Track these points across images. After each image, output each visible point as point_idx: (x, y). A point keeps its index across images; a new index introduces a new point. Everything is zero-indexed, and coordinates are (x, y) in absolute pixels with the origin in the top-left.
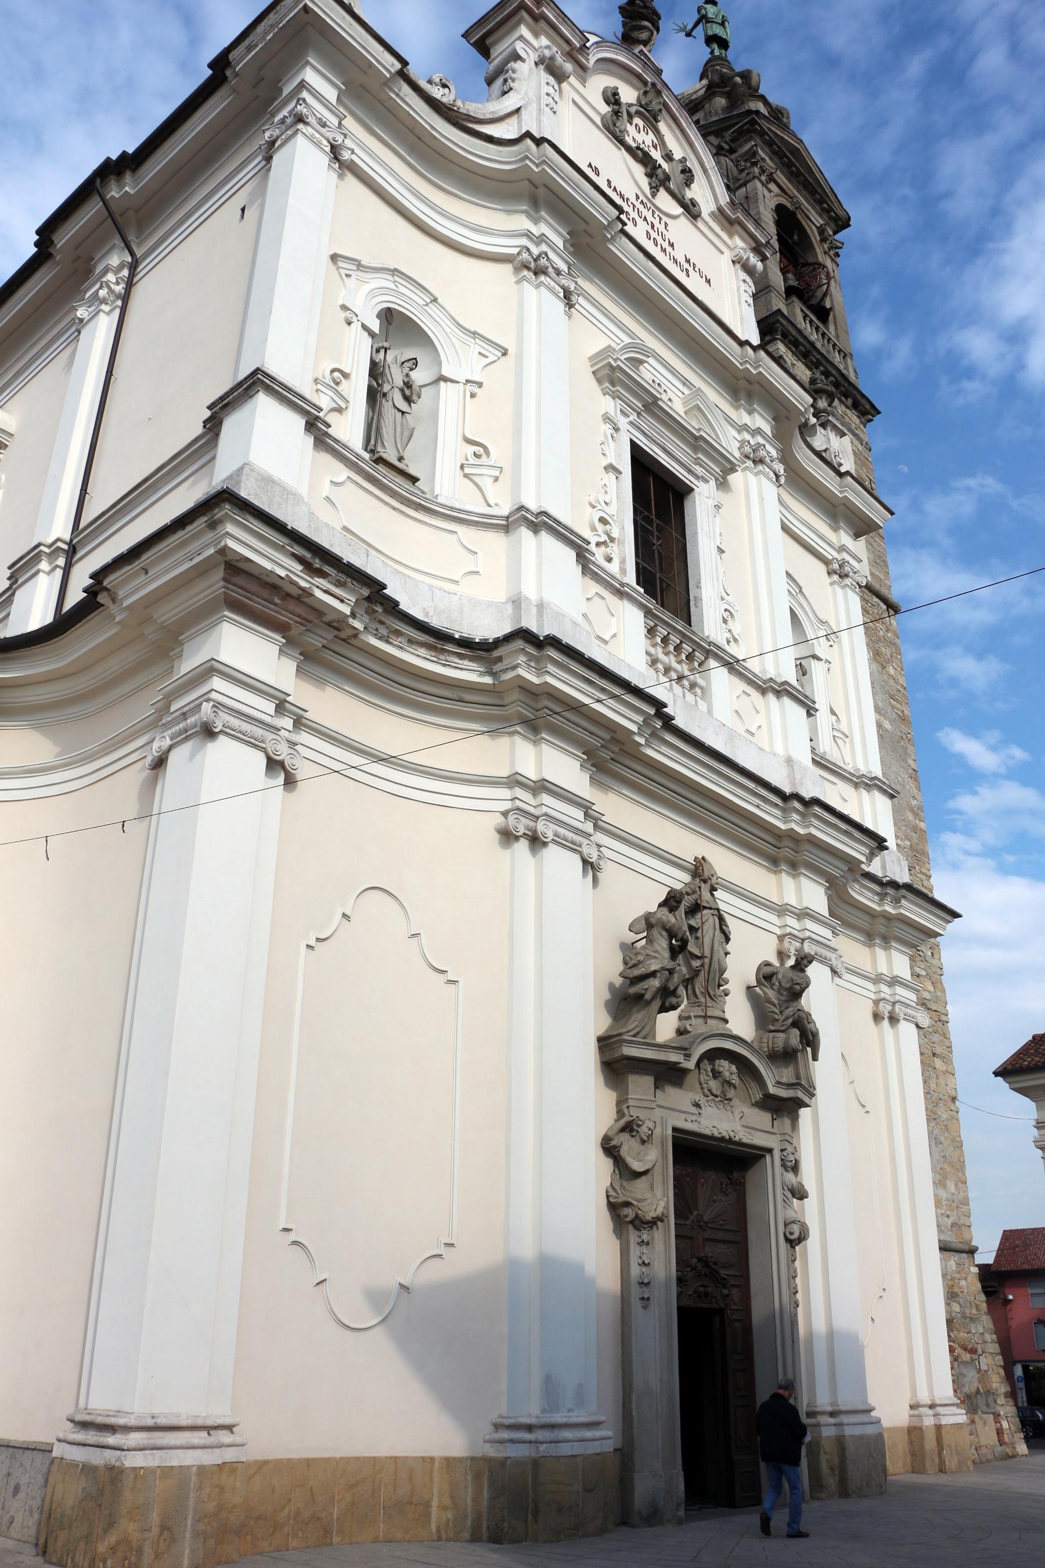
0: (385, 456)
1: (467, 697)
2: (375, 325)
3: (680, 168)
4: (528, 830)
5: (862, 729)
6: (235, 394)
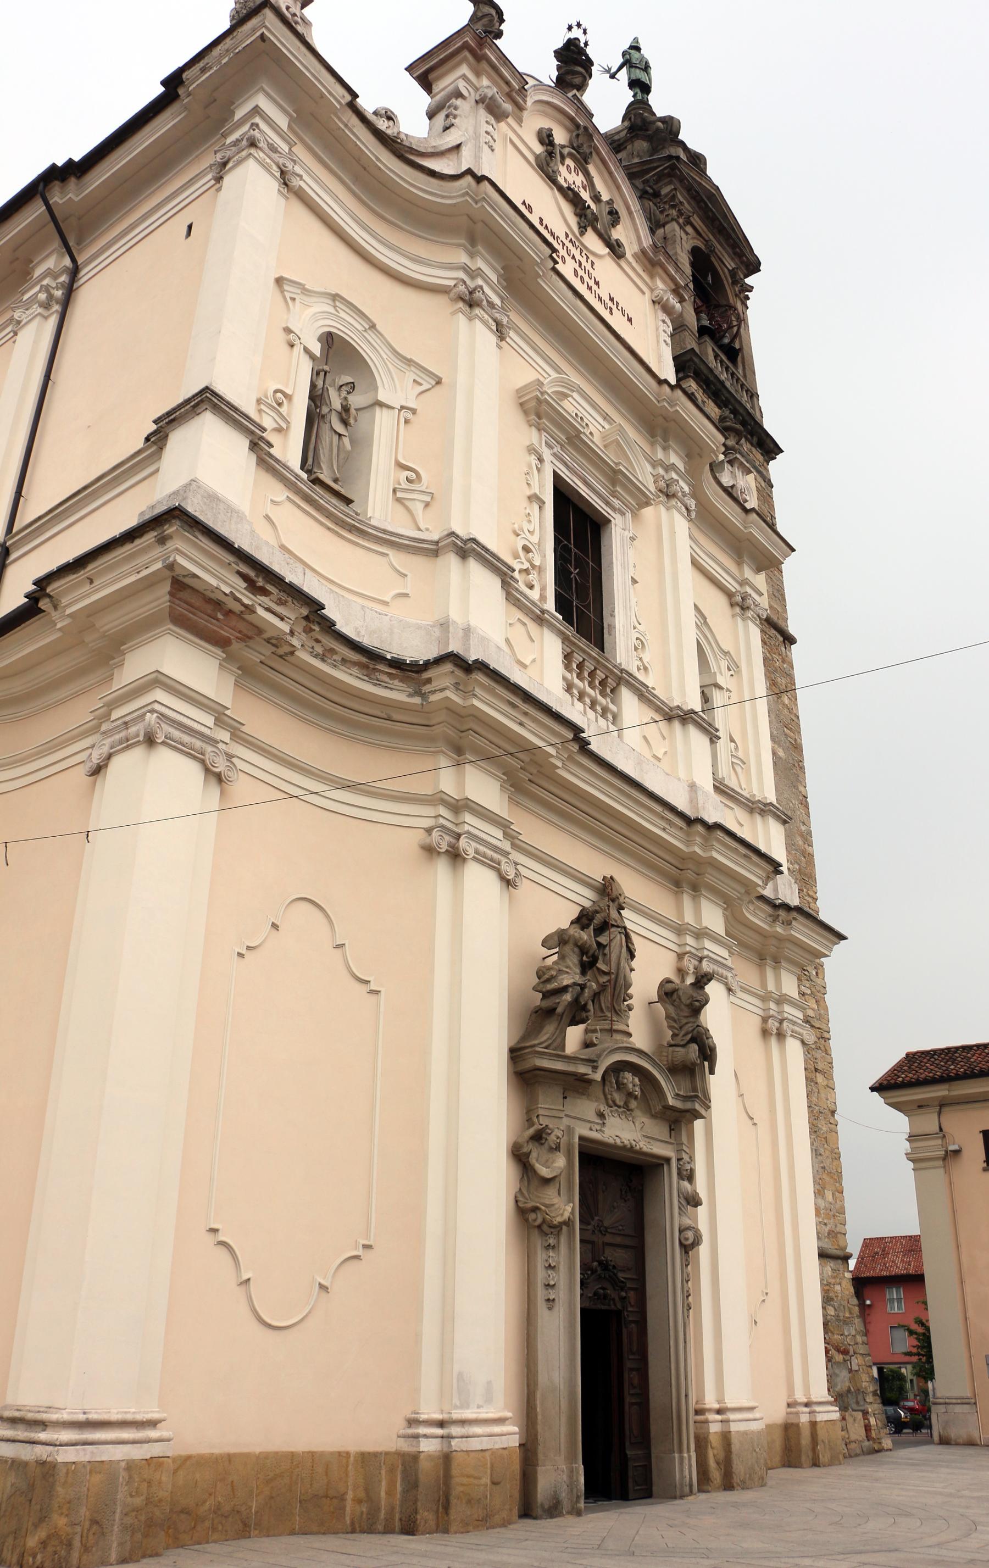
0: (322, 477)
1: (395, 717)
2: (316, 349)
3: (607, 210)
4: (451, 847)
5: (758, 755)
6: (182, 410)
